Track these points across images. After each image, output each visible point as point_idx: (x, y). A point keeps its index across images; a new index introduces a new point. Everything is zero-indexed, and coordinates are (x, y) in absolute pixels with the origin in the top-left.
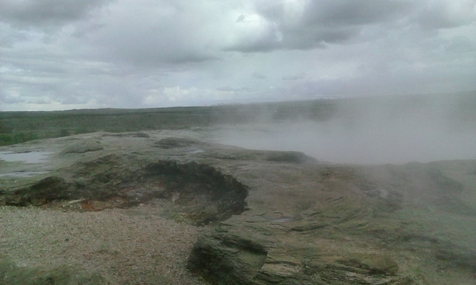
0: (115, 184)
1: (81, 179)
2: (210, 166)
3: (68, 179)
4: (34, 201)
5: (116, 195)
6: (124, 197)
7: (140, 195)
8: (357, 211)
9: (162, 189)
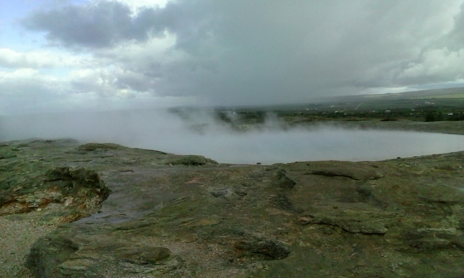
0: (15, 190)
5: (16, 201)
6: (24, 203)
7: (38, 201)
9: (59, 194)
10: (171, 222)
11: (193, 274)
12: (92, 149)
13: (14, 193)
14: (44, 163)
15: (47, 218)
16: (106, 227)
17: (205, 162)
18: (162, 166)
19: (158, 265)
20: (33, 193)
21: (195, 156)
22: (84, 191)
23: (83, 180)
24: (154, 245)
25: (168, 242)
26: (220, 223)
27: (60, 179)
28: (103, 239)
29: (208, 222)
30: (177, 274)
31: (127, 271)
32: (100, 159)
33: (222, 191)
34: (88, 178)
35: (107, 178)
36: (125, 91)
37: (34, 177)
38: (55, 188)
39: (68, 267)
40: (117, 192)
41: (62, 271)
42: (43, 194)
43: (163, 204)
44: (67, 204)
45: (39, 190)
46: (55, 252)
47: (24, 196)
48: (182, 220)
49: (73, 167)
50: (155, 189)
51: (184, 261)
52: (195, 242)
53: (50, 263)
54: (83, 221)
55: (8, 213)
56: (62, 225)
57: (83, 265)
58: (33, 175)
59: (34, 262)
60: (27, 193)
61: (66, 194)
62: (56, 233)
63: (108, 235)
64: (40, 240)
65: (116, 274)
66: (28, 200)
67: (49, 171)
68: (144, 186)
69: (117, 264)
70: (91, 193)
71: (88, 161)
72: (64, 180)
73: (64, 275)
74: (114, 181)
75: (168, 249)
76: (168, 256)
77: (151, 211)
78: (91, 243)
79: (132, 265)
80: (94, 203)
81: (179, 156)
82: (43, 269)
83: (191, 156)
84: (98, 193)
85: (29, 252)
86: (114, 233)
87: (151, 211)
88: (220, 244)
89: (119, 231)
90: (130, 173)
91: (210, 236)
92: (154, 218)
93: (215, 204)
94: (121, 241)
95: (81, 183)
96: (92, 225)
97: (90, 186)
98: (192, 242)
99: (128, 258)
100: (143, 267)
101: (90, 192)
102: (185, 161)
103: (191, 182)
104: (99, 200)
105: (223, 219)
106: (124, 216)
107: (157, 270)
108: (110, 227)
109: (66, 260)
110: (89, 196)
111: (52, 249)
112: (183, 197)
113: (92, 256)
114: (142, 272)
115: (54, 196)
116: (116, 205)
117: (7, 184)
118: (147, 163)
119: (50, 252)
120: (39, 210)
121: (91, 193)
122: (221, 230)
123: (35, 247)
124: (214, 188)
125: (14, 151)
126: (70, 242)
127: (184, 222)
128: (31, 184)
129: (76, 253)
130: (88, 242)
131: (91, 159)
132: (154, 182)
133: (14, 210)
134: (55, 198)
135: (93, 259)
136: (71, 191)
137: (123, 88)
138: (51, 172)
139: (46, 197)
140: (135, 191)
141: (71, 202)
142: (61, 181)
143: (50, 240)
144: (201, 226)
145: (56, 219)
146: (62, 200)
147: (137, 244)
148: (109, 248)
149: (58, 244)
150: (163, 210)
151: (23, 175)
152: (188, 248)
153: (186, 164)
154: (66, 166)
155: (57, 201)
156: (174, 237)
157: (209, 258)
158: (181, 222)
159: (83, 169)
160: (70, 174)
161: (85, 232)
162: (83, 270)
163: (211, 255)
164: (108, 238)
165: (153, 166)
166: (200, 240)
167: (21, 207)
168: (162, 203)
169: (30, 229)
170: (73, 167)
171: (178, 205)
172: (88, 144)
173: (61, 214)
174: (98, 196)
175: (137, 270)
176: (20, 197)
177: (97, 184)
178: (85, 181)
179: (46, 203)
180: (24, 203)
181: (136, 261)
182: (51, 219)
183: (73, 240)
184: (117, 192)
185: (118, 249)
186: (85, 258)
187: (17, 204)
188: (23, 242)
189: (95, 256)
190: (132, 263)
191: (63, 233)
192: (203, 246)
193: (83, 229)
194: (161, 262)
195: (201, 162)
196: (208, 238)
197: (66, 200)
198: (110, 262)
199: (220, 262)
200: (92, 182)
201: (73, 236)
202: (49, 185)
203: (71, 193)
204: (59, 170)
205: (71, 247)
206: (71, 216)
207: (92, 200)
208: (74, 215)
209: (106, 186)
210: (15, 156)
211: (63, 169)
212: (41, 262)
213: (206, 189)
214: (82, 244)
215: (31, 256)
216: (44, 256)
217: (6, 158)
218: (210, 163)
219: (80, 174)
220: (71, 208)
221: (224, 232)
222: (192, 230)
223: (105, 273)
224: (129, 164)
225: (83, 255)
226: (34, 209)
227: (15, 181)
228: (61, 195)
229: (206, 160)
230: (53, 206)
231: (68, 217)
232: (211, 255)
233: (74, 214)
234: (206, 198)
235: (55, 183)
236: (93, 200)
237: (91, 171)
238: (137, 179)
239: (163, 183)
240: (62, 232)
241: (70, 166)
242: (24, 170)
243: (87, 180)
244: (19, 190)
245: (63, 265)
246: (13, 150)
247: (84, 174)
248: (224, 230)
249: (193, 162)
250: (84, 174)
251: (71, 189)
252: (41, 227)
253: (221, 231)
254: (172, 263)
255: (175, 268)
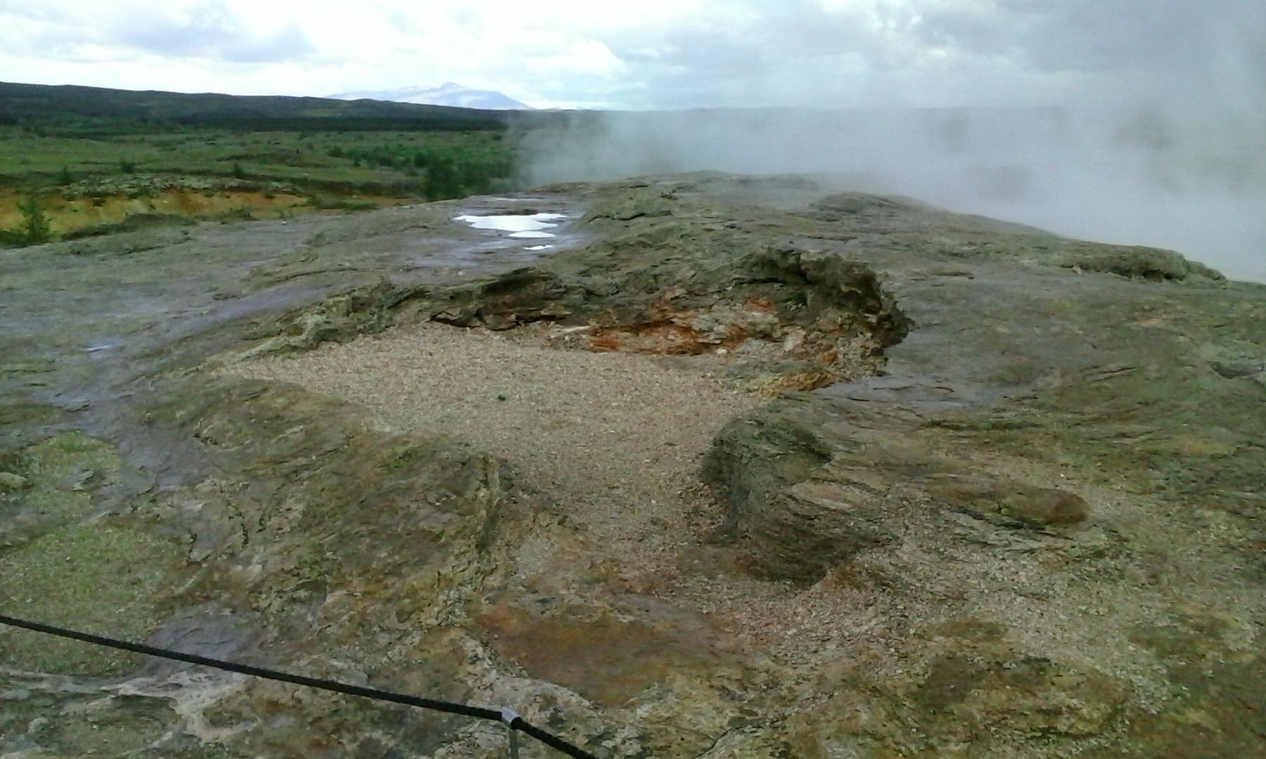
0: (669, 296)
1: (597, 280)
2: (869, 268)
3: (569, 276)
4: (489, 319)
5: (670, 323)
6: (687, 330)
7: (721, 328)
8: (1147, 404)
9: (771, 318)
10: (1083, 429)
11: (1152, 580)
12: (852, 208)
13: (667, 303)
14: (737, 236)
15: (743, 373)
16: (902, 413)
17: (1183, 270)
18: (1051, 269)
19: (1053, 536)
20: (709, 308)
21: (1156, 251)
22: (833, 316)
23: (835, 286)
24: (1034, 482)
25: (1075, 482)
26: (1239, 452)
27: (776, 281)
28: (895, 442)
29: (1199, 446)
30: (1106, 572)
31: (963, 537)
32: (876, 237)
33: (1246, 362)
34: (847, 284)
35: (900, 288)
36: (939, 53)
37: (713, 268)
38: (763, 301)
39: (808, 498)
40: (929, 326)
41: (792, 504)
42: (733, 315)
43: (1063, 375)
44: (789, 345)
45: (724, 301)
46: (772, 456)
47: (688, 314)
48: (1118, 427)
49: (811, 252)
50: (1037, 331)
51: (1126, 540)
52: (1154, 496)
53: (760, 480)
54: (838, 391)
55: (652, 351)
56: (787, 392)
57: (845, 501)
58: (712, 264)
59: (721, 472)
60: (696, 308)
61: (788, 320)
62: (775, 410)
63: (908, 435)
64: (735, 421)
65: (931, 539)
66: (696, 325)
67: (750, 256)
68: (1006, 319)
69: (935, 512)
70: (850, 325)
71: (845, 239)
72: (784, 283)
73: (796, 515)
74: (921, 296)
75: (1080, 500)
76: (1082, 517)
77: (1025, 391)
78: (863, 447)
79: (976, 523)
80: (860, 351)
81: (1105, 248)
82: (744, 493)
83: (1139, 251)
84: (871, 328)
85: (707, 447)
86: (921, 432)
87: (1025, 391)
88: (1235, 513)
89: (937, 430)
90: (964, 279)
91: (1201, 486)
92: (1033, 410)
93: (1222, 398)
94: (941, 455)
95: (829, 295)
96: (865, 405)
97: (851, 305)
98: (1144, 493)
99: (966, 502)
100: (1006, 534)
101: (849, 321)
102: (1123, 264)
103: (1146, 324)
104: (872, 345)
105: (1250, 444)
106: (948, 395)
107: (1049, 549)
108: (911, 417)
109: (800, 479)
110: (846, 331)
111: (765, 447)
112: (1123, 365)
113: (867, 482)
114: (1006, 546)
115: (758, 320)
116: (925, 361)
117: (652, 280)
118: (1009, 257)
119: (762, 455)
120: (721, 351)
121: (850, 325)
122: (1239, 473)
123: (725, 438)
124: (1221, 349)
125: (666, 200)
126: (809, 438)
127: (1124, 435)
128: (706, 285)
129: (826, 466)
130: (857, 444)
131: (852, 235)
132: (1036, 312)
133: (664, 345)
134: (761, 327)
135: (870, 490)
136: (801, 314)
137: (932, 42)
138: (753, 260)
139: (739, 322)
140: (979, 331)
141: (799, 342)
142: (776, 286)
143: (760, 424)
144: (1177, 454)
145: (766, 379)
146: (778, 334)
147: (988, 470)
148: (915, 470)
149: (780, 437)
150: (1061, 392)
151: (689, 261)
152: (1133, 508)
153: (1125, 272)
154: (792, 246)
155: (766, 336)
156: (1092, 470)
157: (1198, 547)
158: (1113, 433)
159: (837, 259)
160: (803, 267)
161: (848, 419)
162: (844, 513)
163: (1204, 539)
164: (907, 443)
165: (1025, 269)
166: (1172, 492)
167: (680, 340)
168: (1057, 373)
169: (705, 393)
170: (812, 251)
171: (1106, 384)
172: (844, 194)
173: (778, 369)
174: (869, 335)
175: (992, 538)
176: (680, 315)
177: (871, 303)
178: (840, 291)
179: (737, 337)
180: (687, 330)
181: (989, 515)
182: (753, 378)
183: (818, 433)
184: (929, 326)
185: (935, 475)
186: (849, 482)
187: (672, 331)
188: (692, 422)
189: (875, 482)
190: (977, 517)
191: (792, 412)
192: (1179, 511)
193: (841, 409)
194: (1061, 530)
195: (1172, 269)
196: (1198, 491)
197: (787, 334)
198: (917, 505)
199: (1233, 563)
200: (861, 294)
201: (818, 425)
202: (746, 291)
203: (800, 318)
204: (776, 257)
205: (812, 451)
206: (802, 377)
207: (853, 344)
208: (809, 374)
209: (900, 307)
210: (668, 213)
211: (785, 254)
212: (736, 474)
213: (1195, 350)
214: (840, 447)
215: (714, 456)
216: (744, 461)
217: (648, 216)
218: (1201, 278)
219: (829, 271)
220: (799, 356)
221: (1250, 484)
222: (1148, 459)
223: (903, 529)
224: (955, 255)
225: (843, 474)
226: (708, 346)
227: (670, 274)
228: (776, 320)
229: (1189, 266)
230: (754, 346)
231: (796, 378)
232: (1204, 539)
233: (811, 370)
234: (1194, 376)
235: (762, 288)
236: (857, 343)
237: (857, 266)
238: (986, 299)
239: (1061, 318)
240: (791, 410)
241: (804, 248)
242: (690, 248)
243: (844, 289)
244: (677, 297)
245: (794, 490)
246: (664, 196)
247: (839, 271)
248: (1248, 475)
249: (1148, 267)
250: (839, 271)
251: (800, 309)
252: (729, 392)
253: (1239, 478)
254: (1093, 539)
255: (1100, 554)
